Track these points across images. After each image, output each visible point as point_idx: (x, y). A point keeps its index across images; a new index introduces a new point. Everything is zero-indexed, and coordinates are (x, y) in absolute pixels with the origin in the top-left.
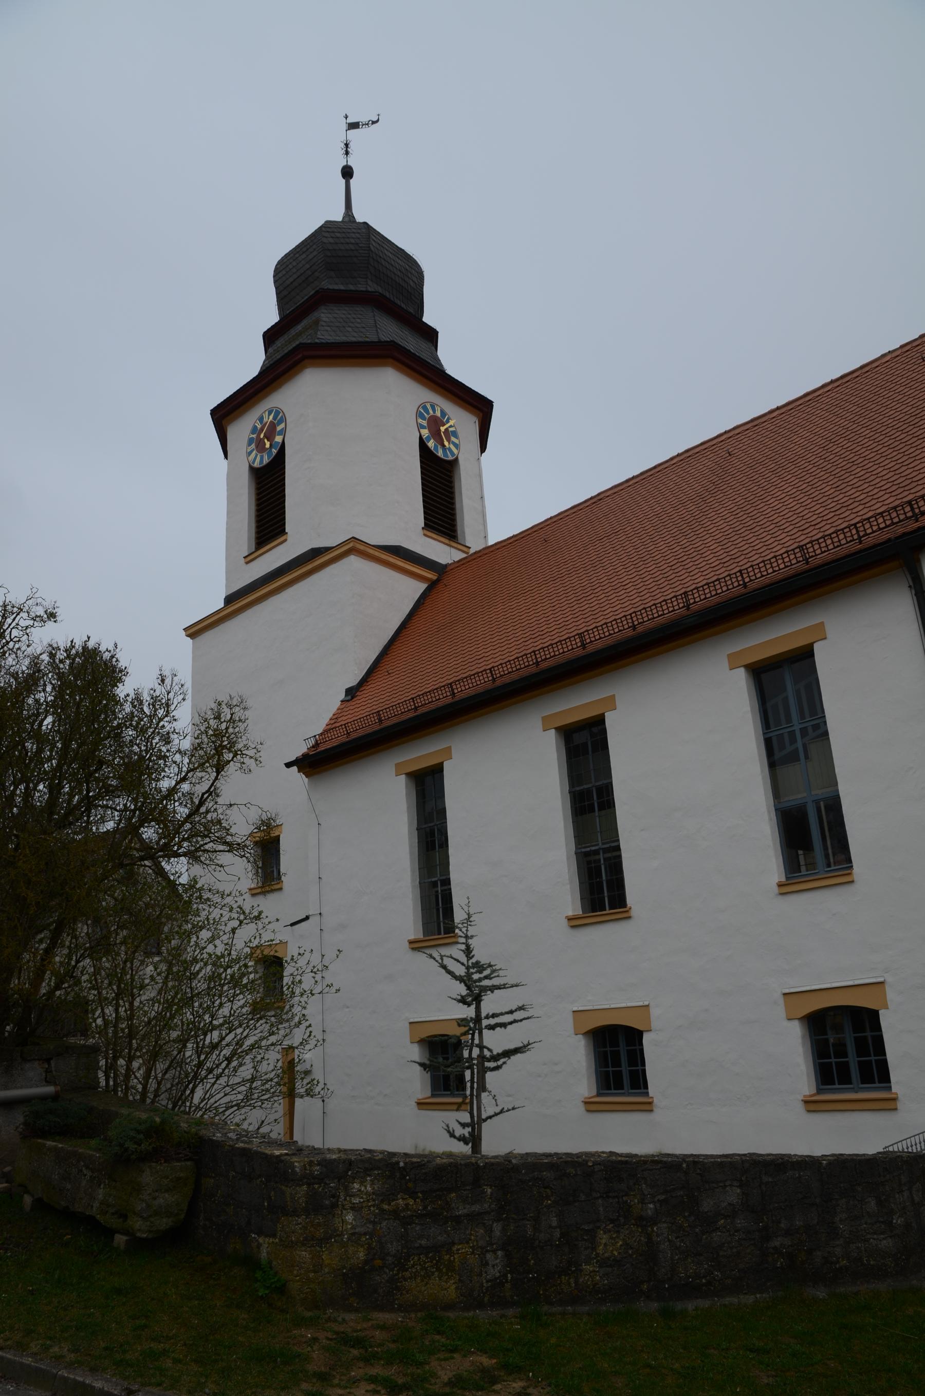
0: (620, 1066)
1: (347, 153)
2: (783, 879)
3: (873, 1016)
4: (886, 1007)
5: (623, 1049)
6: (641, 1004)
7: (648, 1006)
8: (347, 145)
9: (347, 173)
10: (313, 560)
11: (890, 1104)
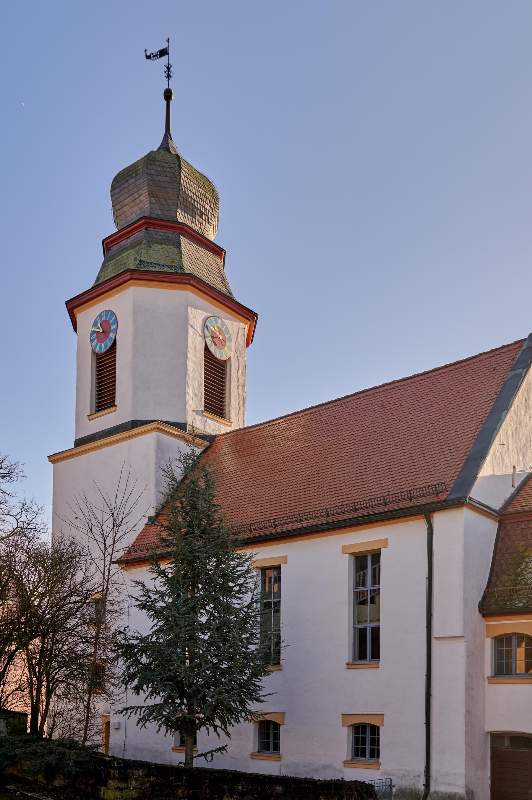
1: (169, 76)
2: (351, 661)
3: (277, 726)
4: (383, 726)
5: (271, 732)
6: (379, 713)
7: (383, 715)
8: (168, 68)
9: (168, 95)
11: (279, 758)
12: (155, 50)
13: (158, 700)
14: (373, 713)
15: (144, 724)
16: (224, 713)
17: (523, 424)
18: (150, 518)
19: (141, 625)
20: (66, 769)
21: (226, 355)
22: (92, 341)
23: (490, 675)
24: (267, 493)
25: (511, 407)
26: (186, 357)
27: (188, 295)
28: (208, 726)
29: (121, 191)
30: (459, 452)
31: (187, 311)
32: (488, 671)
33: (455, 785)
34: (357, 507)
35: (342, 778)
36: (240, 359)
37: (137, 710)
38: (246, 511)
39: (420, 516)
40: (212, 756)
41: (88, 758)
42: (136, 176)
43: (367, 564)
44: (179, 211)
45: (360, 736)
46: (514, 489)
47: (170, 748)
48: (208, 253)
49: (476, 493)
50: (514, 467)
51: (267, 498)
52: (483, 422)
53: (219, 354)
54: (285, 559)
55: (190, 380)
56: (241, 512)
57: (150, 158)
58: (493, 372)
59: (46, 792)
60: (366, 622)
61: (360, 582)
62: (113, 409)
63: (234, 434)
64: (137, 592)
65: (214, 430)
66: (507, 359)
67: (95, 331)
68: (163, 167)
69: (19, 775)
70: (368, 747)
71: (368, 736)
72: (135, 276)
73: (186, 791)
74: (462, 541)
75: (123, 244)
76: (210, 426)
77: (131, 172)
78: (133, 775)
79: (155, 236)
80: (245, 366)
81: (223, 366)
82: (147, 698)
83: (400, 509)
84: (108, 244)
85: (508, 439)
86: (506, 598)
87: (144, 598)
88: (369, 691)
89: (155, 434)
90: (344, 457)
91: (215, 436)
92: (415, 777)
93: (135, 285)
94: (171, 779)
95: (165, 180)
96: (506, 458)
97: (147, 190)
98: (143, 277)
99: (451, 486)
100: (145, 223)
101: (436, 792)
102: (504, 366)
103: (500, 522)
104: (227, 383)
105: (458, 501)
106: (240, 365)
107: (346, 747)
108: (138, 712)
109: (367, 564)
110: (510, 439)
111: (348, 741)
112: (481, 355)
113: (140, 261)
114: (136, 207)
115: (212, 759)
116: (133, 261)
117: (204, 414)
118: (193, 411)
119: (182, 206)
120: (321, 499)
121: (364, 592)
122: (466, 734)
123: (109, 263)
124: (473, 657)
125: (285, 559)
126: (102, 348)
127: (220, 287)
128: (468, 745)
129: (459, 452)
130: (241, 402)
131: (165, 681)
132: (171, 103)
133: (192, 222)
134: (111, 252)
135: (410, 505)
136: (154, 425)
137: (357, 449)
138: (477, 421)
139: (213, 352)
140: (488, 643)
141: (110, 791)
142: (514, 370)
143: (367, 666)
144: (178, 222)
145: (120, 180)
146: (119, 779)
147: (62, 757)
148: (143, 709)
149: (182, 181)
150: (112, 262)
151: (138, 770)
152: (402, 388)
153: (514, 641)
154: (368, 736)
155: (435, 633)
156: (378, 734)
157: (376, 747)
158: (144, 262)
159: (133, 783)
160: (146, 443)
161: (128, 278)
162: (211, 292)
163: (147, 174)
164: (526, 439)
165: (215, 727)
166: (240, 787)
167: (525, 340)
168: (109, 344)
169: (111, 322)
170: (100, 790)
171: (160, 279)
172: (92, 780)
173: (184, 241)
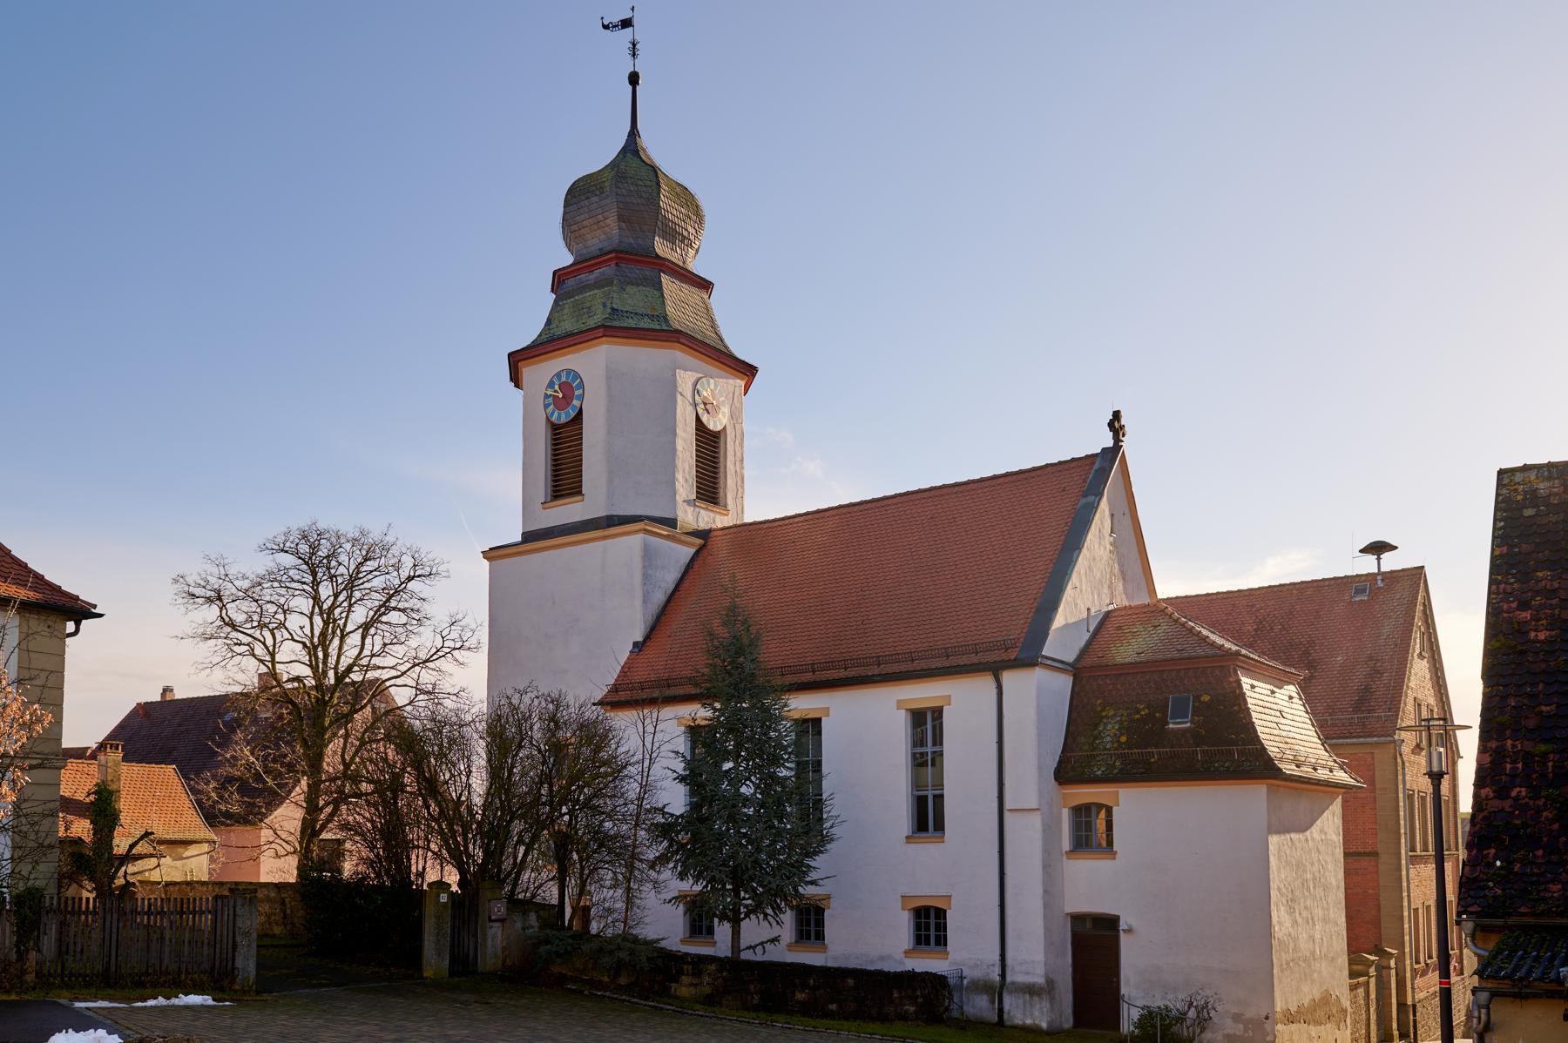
3: (820, 911)
9: (634, 79)
12: (616, 19)
18: (636, 644)
22: (546, 406)
26: (675, 434)
27: (677, 354)
32: (1066, 844)
43: (926, 726)
53: (713, 424)
54: (827, 711)
55: (679, 463)
61: (918, 741)
70: (932, 933)
71: (932, 921)
74: (1035, 701)
84: (560, 279)
88: (930, 870)
89: (640, 536)
91: (710, 531)
101: (1013, 983)
103: (1075, 676)
105: (1029, 657)
109: (926, 726)
124: (1050, 831)
125: (827, 711)
126: (563, 417)
128: (1047, 929)
146: (693, 975)
147: (632, 953)
153: (1094, 810)
154: (932, 921)
155: (1008, 805)
159: (706, 979)
160: (627, 546)
165: (766, 915)
168: (573, 414)
173: (665, 279)
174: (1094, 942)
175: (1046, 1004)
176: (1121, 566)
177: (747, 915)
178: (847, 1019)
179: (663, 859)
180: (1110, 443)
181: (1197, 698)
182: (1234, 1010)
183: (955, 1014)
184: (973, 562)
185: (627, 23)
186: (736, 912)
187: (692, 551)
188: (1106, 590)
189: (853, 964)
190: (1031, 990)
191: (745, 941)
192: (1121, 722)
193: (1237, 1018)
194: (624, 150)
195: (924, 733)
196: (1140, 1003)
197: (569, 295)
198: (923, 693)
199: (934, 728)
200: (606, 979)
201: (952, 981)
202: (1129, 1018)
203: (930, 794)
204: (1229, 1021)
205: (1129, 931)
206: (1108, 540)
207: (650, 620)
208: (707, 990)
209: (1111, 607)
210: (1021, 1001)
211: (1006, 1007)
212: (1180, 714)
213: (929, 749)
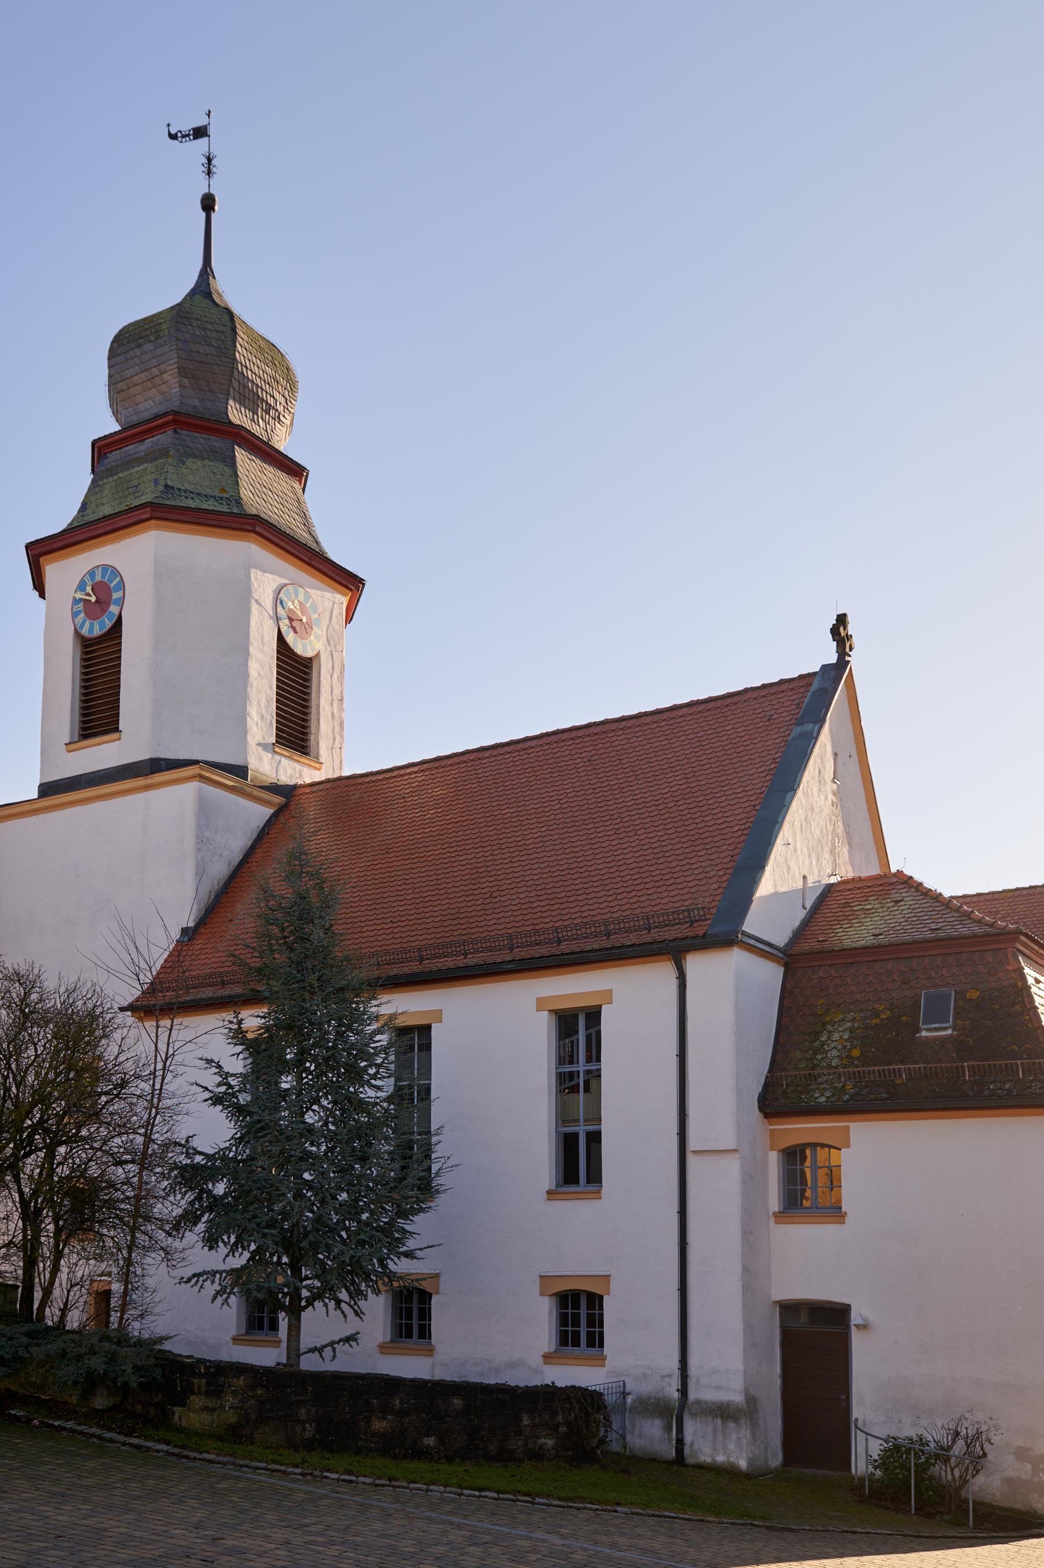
0: (412, 1319)
1: (209, 173)
2: (553, 1187)
3: (425, 1297)
4: (609, 1294)
6: (603, 1273)
7: (609, 1276)
8: (209, 160)
9: (208, 204)
10: (153, 768)
12: (187, 126)
13: (240, 1260)
14: (592, 1273)
15: (226, 1300)
16: (349, 1278)
17: (817, 810)
19: (212, 1131)
20: (121, 1379)
21: (313, 649)
22: (74, 615)
23: (776, 1209)
24: (400, 898)
25: (798, 786)
26: (246, 653)
28: (327, 1301)
29: (127, 360)
30: (722, 855)
31: (248, 576)
32: (774, 1203)
33: (728, 1389)
34: (560, 935)
35: (553, 1383)
36: (336, 655)
37: (214, 1276)
38: (365, 929)
39: (666, 957)
40: (334, 1350)
41: (152, 1361)
42: (157, 339)
43: (577, 1032)
44: (231, 402)
45: (570, 1311)
46: (805, 912)
47: (229, 1337)
48: (280, 474)
49: (753, 924)
50: (804, 877)
51: (402, 908)
52: (757, 807)
53: (302, 647)
54: (438, 1015)
55: (252, 693)
56: (356, 931)
57: (179, 313)
58: (768, 723)
59: (83, 1420)
60: (578, 1121)
61: (565, 1055)
62: (115, 735)
63: (329, 785)
64: (211, 1079)
65: (291, 777)
66: (789, 703)
67: (81, 599)
68: (204, 329)
69: (22, 1391)
70: (583, 1329)
71: (583, 1312)
72: (159, 515)
73: (313, 1411)
74: (730, 995)
75: (132, 452)
76: (286, 771)
77: (148, 333)
78: (230, 1386)
79: (191, 445)
80: (343, 665)
81: (306, 666)
82: (227, 1256)
83: (633, 945)
84: (102, 449)
85: (794, 835)
86: (799, 1088)
87: (223, 1089)
88: (582, 1238)
89: (194, 786)
90: (531, 846)
91: (295, 787)
92: (663, 1377)
93: (158, 528)
94: (289, 1390)
95: (208, 351)
96: (792, 864)
97: (175, 366)
98: (174, 517)
99: (713, 911)
100: (174, 421)
101: (698, 1402)
102: (784, 714)
103: (787, 967)
104: (313, 696)
105: (725, 935)
106: (336, 665)
107: (547, 1331)
108: (217, 1279)
109: (577, 1032)
110: (798, 833)
111: (550, 1321)
112: (746, 690)
113: (166, 486)
114: (154, 390)
115: (334, 1356)
116: (152, 484)
117: (276, 749)
118: (259, 744)
119: (237, 395)
120: (497, 916)
121: (572, 1075)
122: (744, 1305)
123: (105, 481)
124: (751, 1182)
125: (438, 1015)
126: (96, 629)
127: (302, 534)
128: (748, 1325)
129: (722, 855)
130: (337, 729)
131: (263, 1228)
132: (213, 216)
133: (253, 420)
134: (106, 462)
135: (648, 939)
136: (193, 770)
137: (551, 833)
138: (747, 804)
139: (291, 645)
140: (774, 1158)
141: (191, 1415)
142: (799, 724)
143: (580, 1196)
144: (230, 423)
145: (125, 341)
146: (208, 1394)
147: (112, 1359)
148: (224, 1275)
149: (237, 354)
150: (110, 480)
151: (238, 1378)
152: (621, 732)
154: (583, 1312)
155: (692, 1144)
156: (601, 1308)
157: (597, 1329)
158: (173, 488)
159: (230, 1400)
160: (176, 800)
161: (148, 516)
162: (286, 543)
163: (178, 339)
164: (822, 832)
165: (338, 1302)
166: (397, 1402)
167: (814, 674)
168: (109, 624)
169: (112, 585)
170: (173, 1413)
171: (202, 521)
172: (156, 1396)
173: (241, 455)
174: (814, 1340)
175: (745, 1433)
176: (847, 826)
177: (310, 1302)
178: (450, 1460)
179: (189, 1218)
180: (833, 658)
181: (960, 995)
182: (1018, 1442)
183: (615, 1447)
184: (644, 823)
185: (200, 132)
186: (295, 1296)
187: (267, 812)
188: (827, 855)
189: (473, 1376)
190: (724, 1413)
191: (306, 1340)
192: (852, 1030)
193: (1022, 1454)
194: (193, 292)
195: (574, 1046)
196: (882, 1432)
197: (111, 472)
198: (573, 987)
199: (589, 1038)
200: (74, 1400)
201: (610, 1399)
202: (864, 1455)
203: (582, 1130)
204: (1011, 1459)
205: (864, 1327)
206: (830, 787)
207: (205, 897)
208: (232, 1418)
209: (833, 880)
210: (709, 1429)
211: (688, 1437)
212: (937, 1016)
213: (581, 1066)
